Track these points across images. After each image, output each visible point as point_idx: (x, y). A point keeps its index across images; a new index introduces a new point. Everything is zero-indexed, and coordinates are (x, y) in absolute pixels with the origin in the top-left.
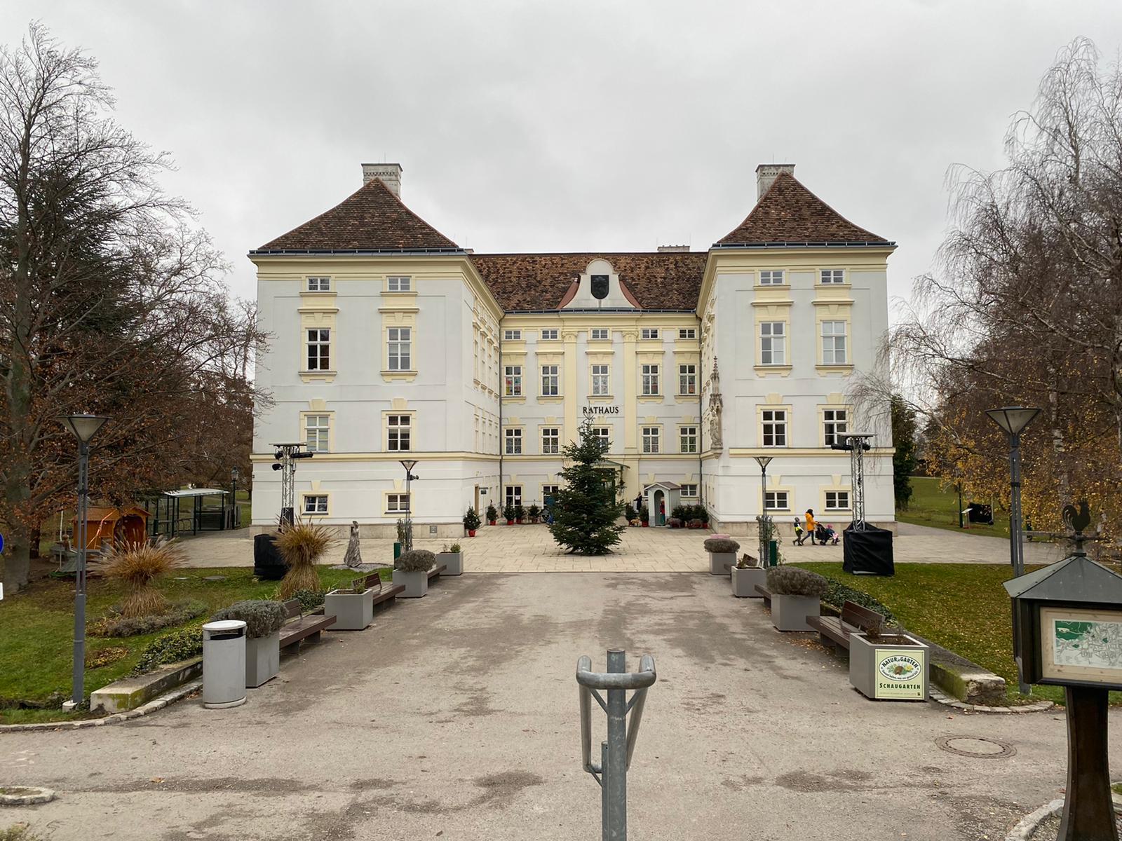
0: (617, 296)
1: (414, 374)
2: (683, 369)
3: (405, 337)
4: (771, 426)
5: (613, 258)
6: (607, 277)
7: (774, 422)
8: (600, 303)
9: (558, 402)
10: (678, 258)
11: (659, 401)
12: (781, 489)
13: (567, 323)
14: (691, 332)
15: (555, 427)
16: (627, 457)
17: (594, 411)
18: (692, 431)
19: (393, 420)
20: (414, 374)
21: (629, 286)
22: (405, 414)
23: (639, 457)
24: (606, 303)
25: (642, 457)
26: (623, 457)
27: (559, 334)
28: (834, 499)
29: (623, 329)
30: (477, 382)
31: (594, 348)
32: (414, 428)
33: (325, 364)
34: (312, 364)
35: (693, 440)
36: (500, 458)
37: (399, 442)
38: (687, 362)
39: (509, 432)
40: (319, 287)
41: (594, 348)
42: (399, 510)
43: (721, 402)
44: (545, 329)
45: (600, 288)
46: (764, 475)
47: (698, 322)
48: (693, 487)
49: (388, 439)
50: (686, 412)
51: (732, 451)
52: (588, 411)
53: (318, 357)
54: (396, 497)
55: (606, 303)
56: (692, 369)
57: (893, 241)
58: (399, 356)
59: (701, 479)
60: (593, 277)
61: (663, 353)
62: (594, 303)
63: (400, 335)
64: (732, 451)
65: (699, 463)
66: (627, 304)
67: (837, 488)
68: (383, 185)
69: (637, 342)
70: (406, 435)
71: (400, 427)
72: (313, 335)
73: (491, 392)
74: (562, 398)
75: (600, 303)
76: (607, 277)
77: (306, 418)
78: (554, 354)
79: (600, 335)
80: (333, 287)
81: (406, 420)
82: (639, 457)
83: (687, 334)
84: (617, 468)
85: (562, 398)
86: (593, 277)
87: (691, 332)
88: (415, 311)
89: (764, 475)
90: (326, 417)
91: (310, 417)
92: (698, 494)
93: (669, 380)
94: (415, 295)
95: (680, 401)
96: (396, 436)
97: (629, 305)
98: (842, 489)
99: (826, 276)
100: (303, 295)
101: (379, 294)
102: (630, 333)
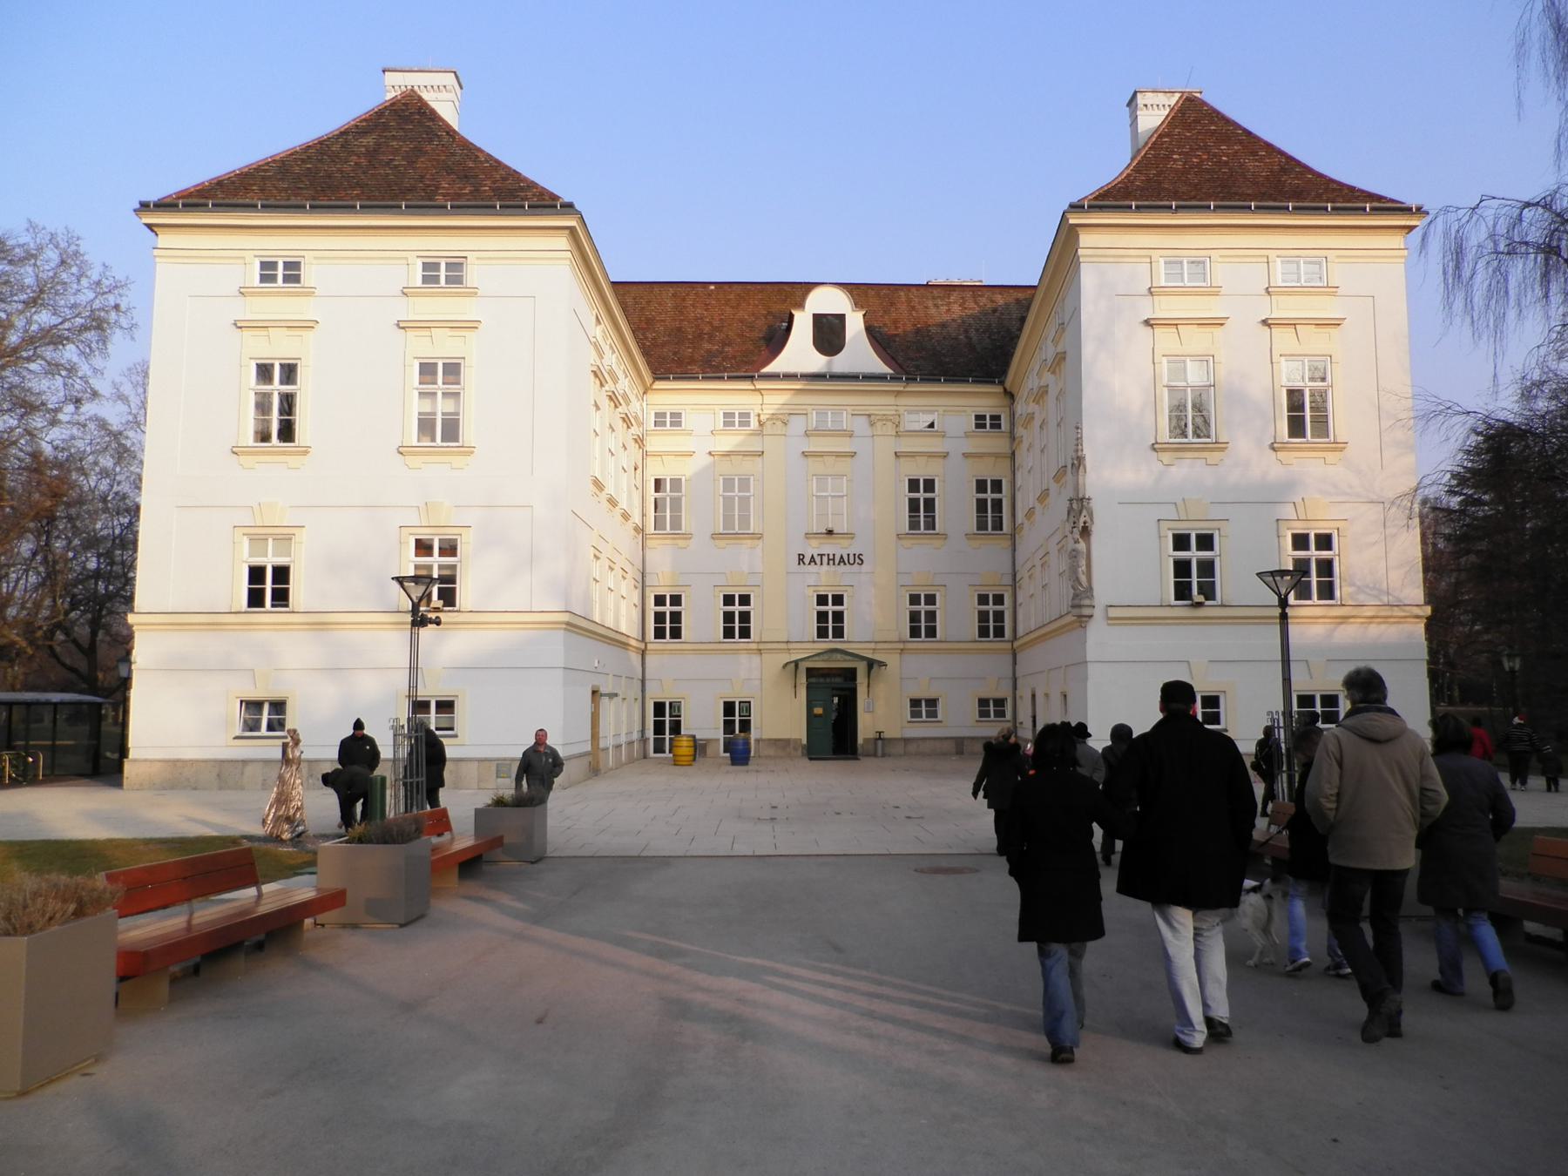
0: (859, 353)
2: (981, 486)
3: (451, 378)
6: (842, 317)
7: (830, 608)
10: (969, 294)
11: (937, 543)
14: (996, 418)
16: (880, 646)
17: (818, 560)
18: (999, 599)
23: (901, 646)
25: (909, 646)
26: (872, 646)
28: (989, 707)
29: (872, 410)
30: (598, 485)
35: (999, 616)
36: (642, 646)
39: (660, 600)
41: (817, 445)
44: (729, 409)
45: (829, 334)
47: (1006, 401)
48: (1000, 703)
50: (988, 561)
51: (1113, 613)
52: (807, 560)
56: (997, 486)
57: (1419, 203)
59: (1015, 688)
60: (818, 318)
61: (945, 456)
62: (817, 362)
63: (441, 373)
64: (1113, 613)
65: (1009, 658)
66: (879, 366)
67: (992, 693)
72: (264, 372)
73: (626, 516)
76: (842, 317)
77: (246, 541)
82: (901, 646)
83: (988, 422)
86: (818, 318)
87: (996, 418)
90: (288, 539)
91: (254, 539)
92: (1009, 715)
93: (956, 507)
97: (886, 370)
98: (999, 695)
99: (267, 271)
101: (397, 290)
102: (885, 419)
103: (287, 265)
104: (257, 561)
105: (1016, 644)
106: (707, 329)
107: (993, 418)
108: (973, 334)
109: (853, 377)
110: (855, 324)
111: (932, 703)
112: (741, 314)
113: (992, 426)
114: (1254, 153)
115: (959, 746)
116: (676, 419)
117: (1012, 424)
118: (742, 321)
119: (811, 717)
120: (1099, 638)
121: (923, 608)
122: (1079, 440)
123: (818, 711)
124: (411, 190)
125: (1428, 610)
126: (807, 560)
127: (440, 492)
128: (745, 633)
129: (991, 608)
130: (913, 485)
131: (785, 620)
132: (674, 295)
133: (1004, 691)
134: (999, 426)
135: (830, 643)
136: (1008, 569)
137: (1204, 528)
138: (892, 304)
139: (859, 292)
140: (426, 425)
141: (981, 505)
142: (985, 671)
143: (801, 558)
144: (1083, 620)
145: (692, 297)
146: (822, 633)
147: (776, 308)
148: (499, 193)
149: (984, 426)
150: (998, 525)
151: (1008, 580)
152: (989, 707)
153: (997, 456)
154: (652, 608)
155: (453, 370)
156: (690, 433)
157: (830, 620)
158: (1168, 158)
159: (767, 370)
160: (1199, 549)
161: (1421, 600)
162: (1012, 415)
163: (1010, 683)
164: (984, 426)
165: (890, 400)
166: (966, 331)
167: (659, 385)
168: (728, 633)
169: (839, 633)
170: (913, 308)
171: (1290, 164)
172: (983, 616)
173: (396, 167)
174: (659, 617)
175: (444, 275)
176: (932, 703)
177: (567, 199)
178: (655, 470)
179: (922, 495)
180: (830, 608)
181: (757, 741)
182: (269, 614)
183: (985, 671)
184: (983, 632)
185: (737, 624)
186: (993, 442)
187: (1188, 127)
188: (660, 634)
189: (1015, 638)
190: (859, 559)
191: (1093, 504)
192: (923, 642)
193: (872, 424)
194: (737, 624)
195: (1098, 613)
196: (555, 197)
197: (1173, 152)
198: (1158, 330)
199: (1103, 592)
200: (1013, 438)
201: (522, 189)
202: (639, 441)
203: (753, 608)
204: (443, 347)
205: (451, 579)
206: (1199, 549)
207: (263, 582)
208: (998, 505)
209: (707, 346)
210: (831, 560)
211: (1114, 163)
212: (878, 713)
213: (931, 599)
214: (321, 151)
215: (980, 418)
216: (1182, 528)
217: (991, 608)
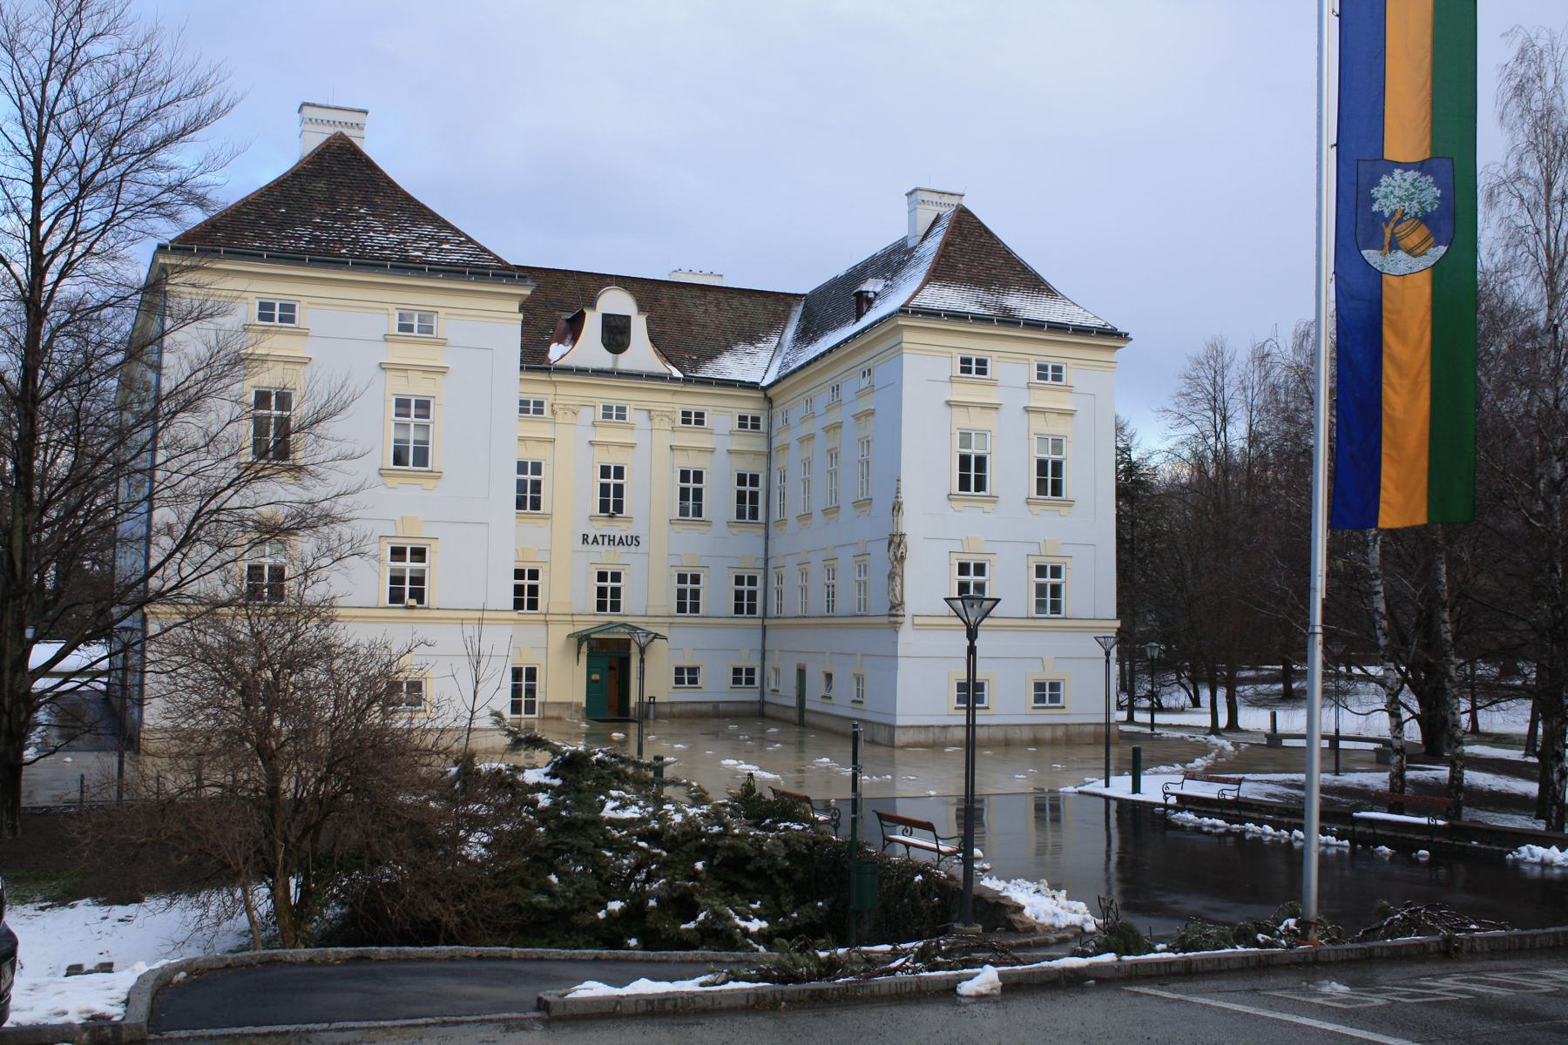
0: (641, 353)
2: (741, 479)
5: (646, 290)
6: (628, 318)
8: (615, 361)
9: (541, 522)
11: (703, 529)
13: (560, 390)
14: (756, 419)
15: (533, 566)
18: (752, 581)
22: (418, 544)
24: (626, 361)
27: (546, 408)
28: (741, 676)
32: (433, 569)
33: (981, 485)
38: (749, 468)
45: (616, 334)
47: (766, 405)
48: (750, 671)
49: (388, 586)
50: (744, 546)
51: (918, 620)
52: (590, 540)
55: (626, 361)
56: (754, 480)
58: (412, 446)
59: (763, 658)
60: (607, 318)
61: (712, 451)
62: (604, 359)
63: (414, 408)
64: (918, 620)
67: (744, 664)
68: (352, 145)
69: (673, 430)
70: (418, 580)
71: (408, 566)
75: (615, 361)
76: (628, 318)
80: (442, 326)
81: (419, 554)
85: (548, 516)
86: (607, 318)
87: (756, 419)
88: (442, 371)
93: (719, 496)
94: (443, 343)
95: (735, 530)
96: (400, 580)
98: (750, 665)
100: (387, 338)
101: (380, 337)
102: (662, 414)
103: (527, 411)
107: (753, 419)
109: (638, 376)
111: (693, 671)
117: (770, 426)
119: (590, 682)
120: (907, 639)
121: (689, 586)
122: (898, 490)
123: (596, 677)
125: (1118, 624)
126: (590, 540)
128: (533, 605)
130: (685, 476)
131: (569, 595)
133: (755, 663)
135: (608, 617)
136: (761, 553)
137: (979, 559)
142: (741, 644)
143: (585, 538)
144: (895, 627)
146: (601, 606)
149: (745, 426)
150: (754, 515)
151: (761, 564)
152: (741, 676)
153: (756, 453)
155: (424, 406)
156: (305, 333)
157: (608, 598)
161: (1114, 614)
163: (759, 655)
165: (668, 398)
169: (616, 607)
176: (693, 671)
179: (691, 485)
181: (543, 704)
183: (741, 644)
186: (752, 442)
189: (765, 617)
190: (636, 541)
191: (908, 539)
192: (687, 618)
193: (651, 419)
195: (907, 620)
199: (910, 607)
203: (540, 582)
204: (416, 388)
210: (612, 540)
212: (654, 681)
213: (696, 579)
215: (742, 418)
216: (965, 558)
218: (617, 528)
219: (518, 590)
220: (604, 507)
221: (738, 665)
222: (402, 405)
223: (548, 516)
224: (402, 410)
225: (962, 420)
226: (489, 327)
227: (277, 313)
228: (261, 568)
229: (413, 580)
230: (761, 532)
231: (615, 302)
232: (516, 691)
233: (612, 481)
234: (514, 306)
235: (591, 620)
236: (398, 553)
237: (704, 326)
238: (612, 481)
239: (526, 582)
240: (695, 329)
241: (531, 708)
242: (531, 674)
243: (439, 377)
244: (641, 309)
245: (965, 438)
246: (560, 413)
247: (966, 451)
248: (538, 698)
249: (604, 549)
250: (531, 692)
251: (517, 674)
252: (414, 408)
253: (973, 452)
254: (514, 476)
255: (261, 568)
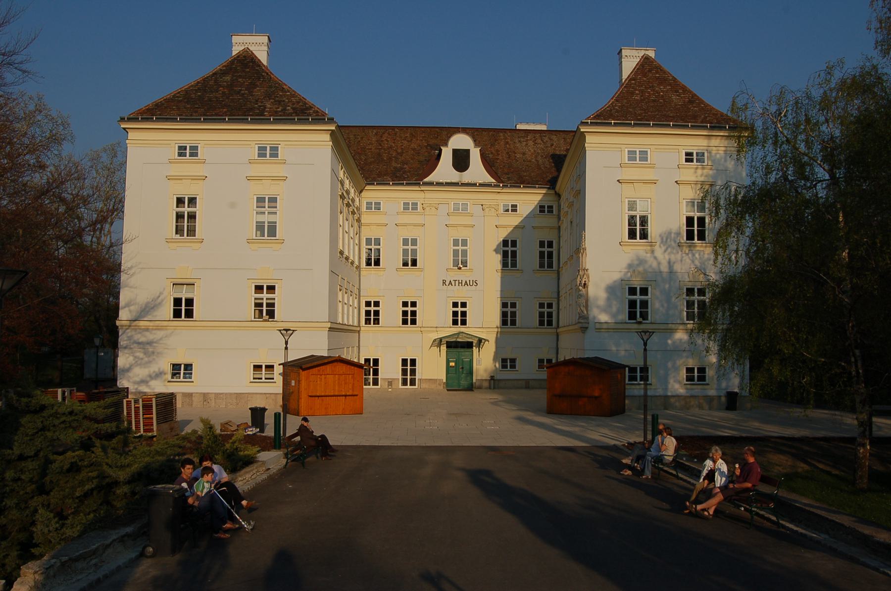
0: (477, 171)
1: (282, 242)
2: (542, 244)
3: (273, 204)
4: (693, 302)
6: (468, 151)
7: (459, 309)
10: (538, 135)
12: (513, 356)
14: (550, 207)
17: (453, 283)
18: (550, 306)
19: (259, 289)
20: (282, 242)
21: (489, 164)
31: (454, 220)
34: (179, 231)
35: (550, 315)
37: (266, 312)
39: (368, 304)
40: (188, 154)
41: (454, 220)
42: (263, 380)
43: (588, 277)
45: (461, 160)
46: (286, 348)
52: (447, 283)
53: (186, 222)
54: (261, 367)
55: (467, 176)
56: (550, 244)
58: (266, 225)
59: (557, 353)
60: (456, 152)
62: (454, 176)
63: (268, 202)
65: (555, 337)
66: (490, 179)
71: (265, 295)
74: (422, 270)
76: (468, 151)
78: (415, 225)
79: (460, 209)
81: (271, 289)
84: (475, 342)
86: (456, 152)
87: (550, 207)
89: (286, 348)
93: (528, 256)
96: (261, 305)
102: (490, 206)
104: (178, 296)
105: (559, 330)
106: (394, 154)
108: (539, 158)
110: (475, 155)
111: (513, 361)
112: (413, 145)
113: (548, 212)
114: (677, 91)
115: (527, 385)
116: (378, 206)
117: (559, 211)
118: (414, 149)
123: (452, 364)
124: (252, 109)
126: (447, 283)
127: (265, 263)
128: (414, 322)
129: (546, 310)
131: (436, 320)
132: (376, 134)
134: (552, 212)
135: (459, 328)
138: (496, 140)
139: (475, 133)
140: (260, 227)
141: (542, 254)
143: (444, 282)
145: (386, 135)
146: (455, 322)
147: (432, 142)
148: (296, 112)
149: (544, 211)
150: (550, 265)
153: (551, 228)
154: (364, 309)
155: (273, 200)
157: (459, 317)
158: (633, 93)
159: (426, 180)
160: (641, 295)
162: (559, 206)
164: (544, 211)
166: (536, 157)
167: (368, 187)
168: (405, 322)
169: (464, 323)
170: (507, 143)
171: (694, 99)
172: (541, 315)
173: (243, 94)
174: (368, 313)
175: (269, 152)
176: (513, 361)
177: (330, 116)
178: (366, 233)
180: (459, 309)
181: (420, 380)
182: (183, 322)
184: (541, 323)
185: (409, 317)
186: (548, 220)
187: (645, 75)
188: (368, 321)
194: (409, 317)
196: (324, 114)
197: (636, 90)
198: (624, 185)
200: (559, 218)
201: (307, 109)
202: (359, 220)
204: (267, 190)
205: (273, 305)
206: (641, 295)
207: (181, 306)
208: (550, 255)
209: (394, 164)
210: (460, 283)
211: (603, 99)
214: (205, 85)
217: (546, 310)
218: (463, 275)
219: (455, 314)
220: (456, 263)
221: (541, 358)
222: (260, 200)
223: (422, 270)
224: (261, 204)
225: (629, 192)
226: (308, 153)
227: (188, 151)
228: (181, 299)
229: (268, 305)
230: (555, 276)
231: (461, 141)
232: (404, 372)
233: (460, 248)
234: (327, 137)
235: (449, 331)
236: (259, 289)
237: (524, 154)
238: (460, 248)
239: (409, 309)
240: (518, 156)
241: (413, 383)
242: (413, 362)
243: (281, 183)
244: (477, 144)
245: (632, 206)
246: (428, 209)
247: (633, 213)
248: (417, 377)
249: (456, 288)
250: (413, 372)
251: (404, 362)
252: (268, 202)
253: (638, 213)
254: (402, 247)
255: (181, 299)
